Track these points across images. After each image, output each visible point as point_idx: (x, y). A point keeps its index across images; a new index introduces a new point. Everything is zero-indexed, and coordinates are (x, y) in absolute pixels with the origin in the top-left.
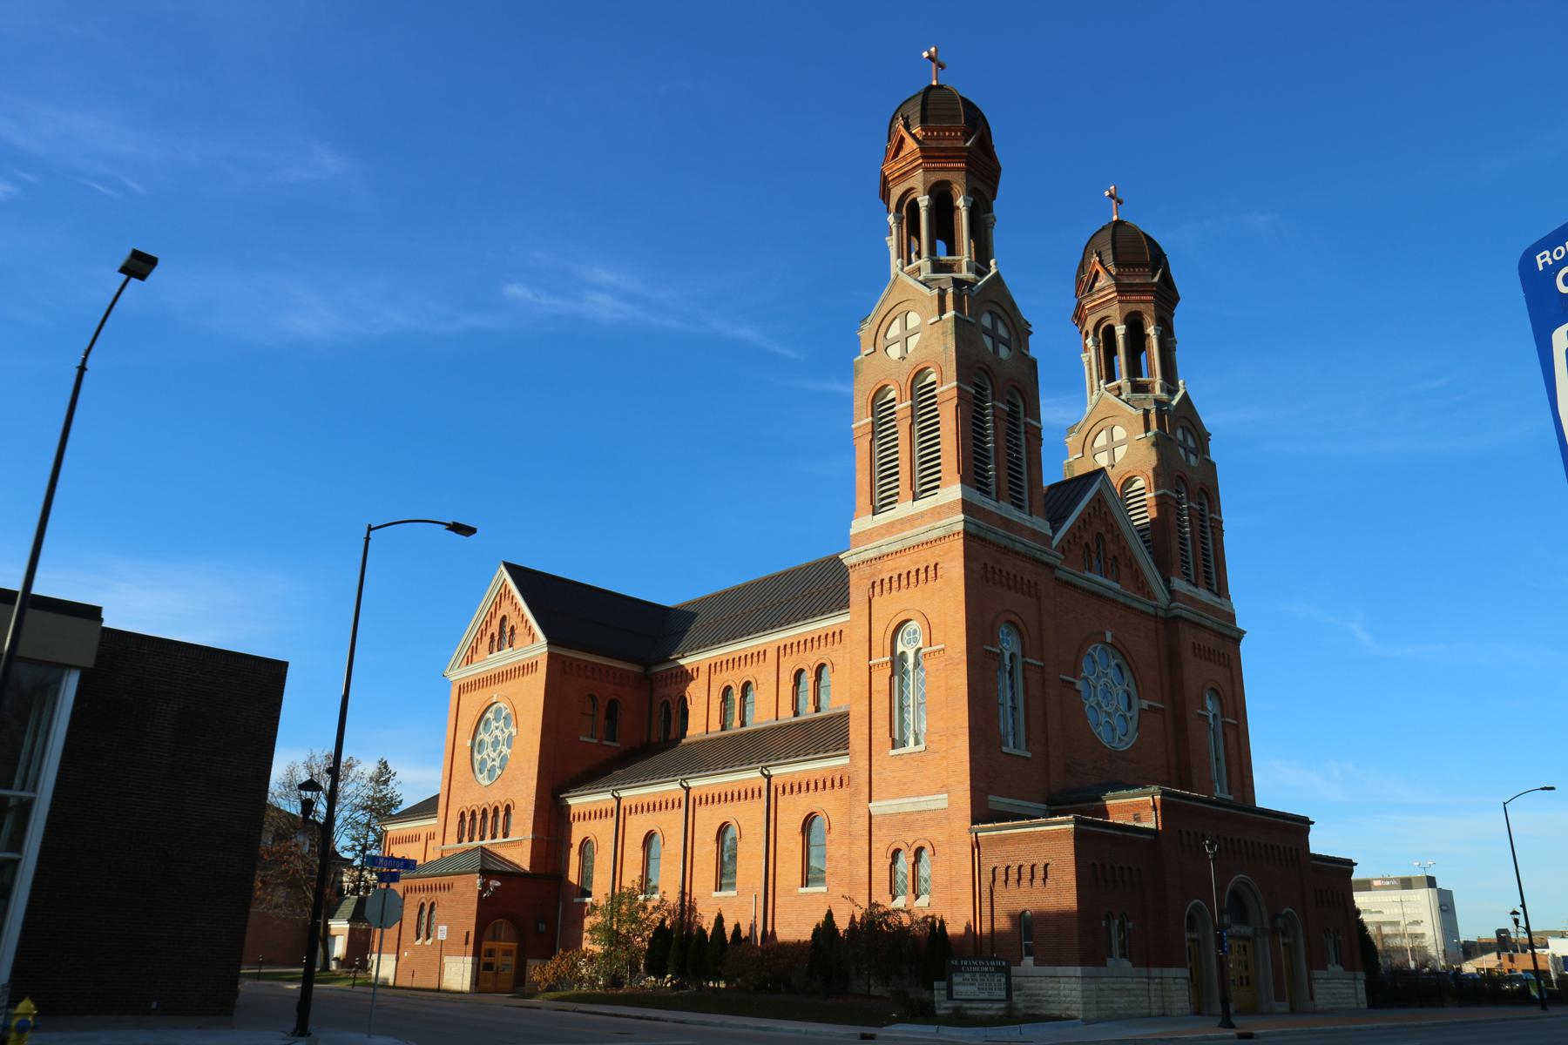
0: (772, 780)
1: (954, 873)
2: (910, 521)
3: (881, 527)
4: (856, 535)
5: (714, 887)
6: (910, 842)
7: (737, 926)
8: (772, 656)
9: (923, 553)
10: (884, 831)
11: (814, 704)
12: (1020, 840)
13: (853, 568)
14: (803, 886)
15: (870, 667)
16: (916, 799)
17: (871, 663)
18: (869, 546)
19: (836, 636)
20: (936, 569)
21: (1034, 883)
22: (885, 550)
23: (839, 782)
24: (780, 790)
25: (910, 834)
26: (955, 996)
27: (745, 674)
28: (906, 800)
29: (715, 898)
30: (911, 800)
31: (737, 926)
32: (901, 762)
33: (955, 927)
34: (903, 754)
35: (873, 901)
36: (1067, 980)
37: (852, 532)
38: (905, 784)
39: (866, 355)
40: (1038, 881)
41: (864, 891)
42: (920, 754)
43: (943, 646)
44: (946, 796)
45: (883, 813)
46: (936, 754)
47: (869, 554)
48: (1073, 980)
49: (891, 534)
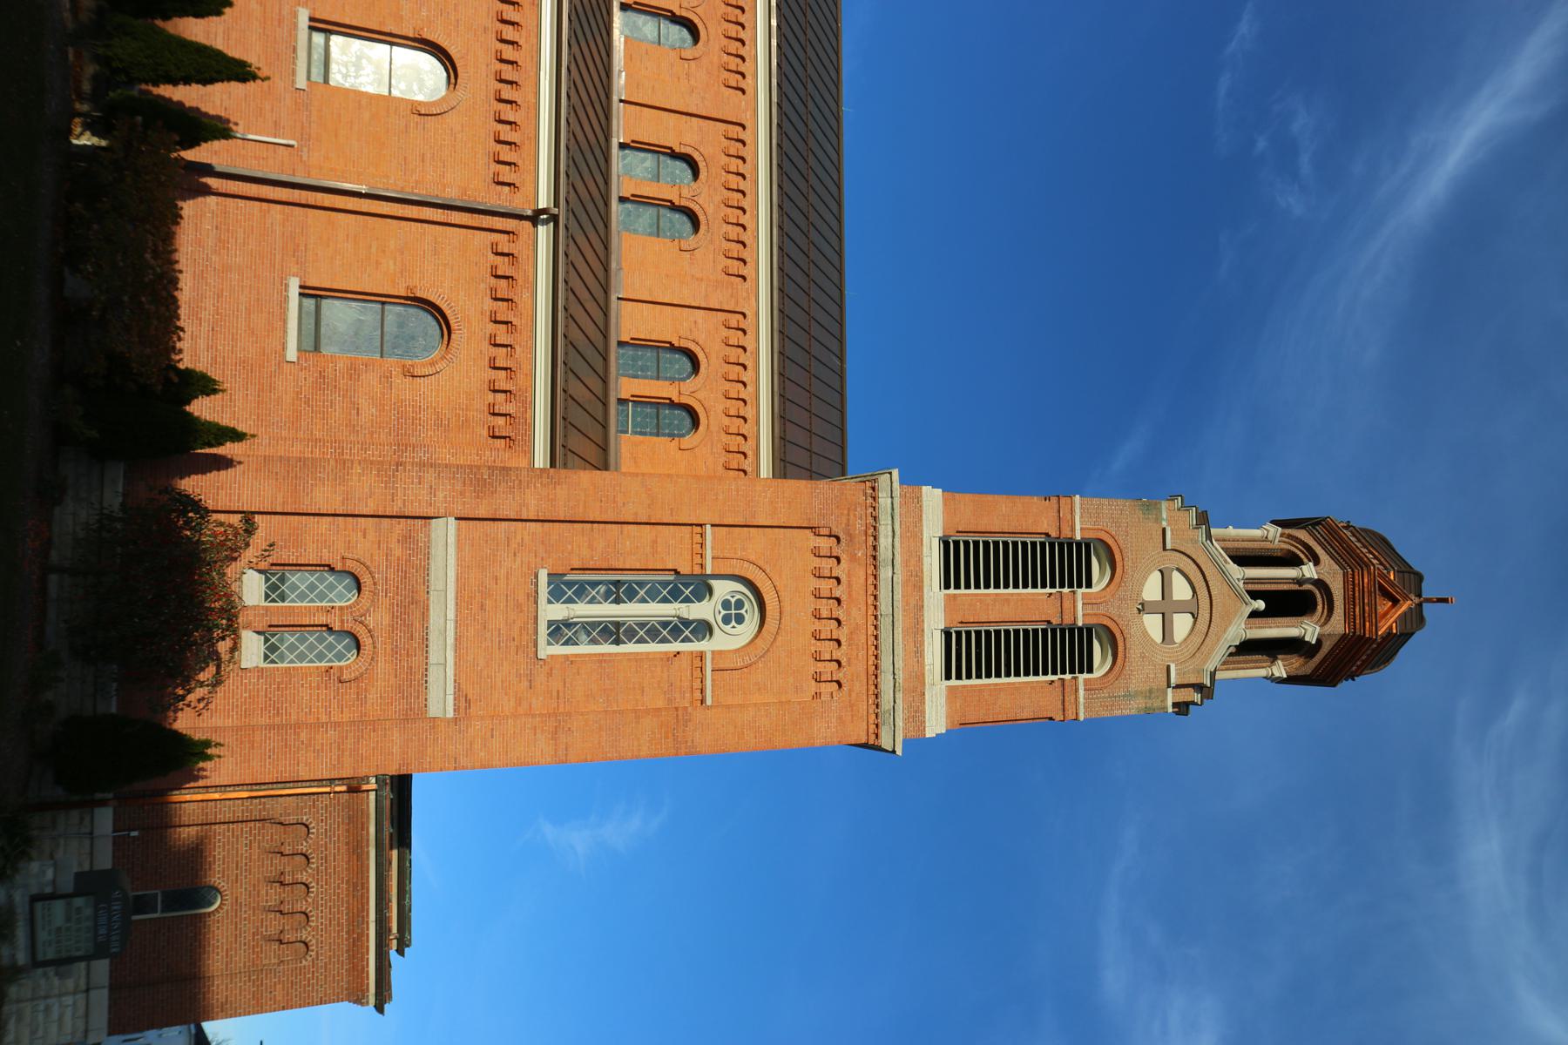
0: (527, 224)
1: (303, 736)
2: (917, 611)
3: (920, 560)
4: (919, 499)
5: (309, 284)
6: (370, 620)
7: (219, 129)
8: (731, 106)
9: (862, 653)
10: (398, 552)
11: (633, 195)
12: (355, 886)
13: (869, 491)
14: (312, 19)
15: (701, 525)
16: (450, 640)
17: (708, 527)
18: (897, 501)
19: (738, 268)
20: (737, 89)
21: (272, 915)
22: (885, 573)
23: (507, 431)
24: (504, 243)
25: (386, 620)
26: (39, 906)
27: (712, 31)
28: (451, 615)
29: (295, 15)
30: (451, 626)
31: (219, 129)
32: (522, 598)
33: (189, 801)
34: (536, 603)
35: (257, 518)
36: (81, 1011)
37: (926, 489)
38: (482, 607)
39: (1164, 530)
40: (273, 924)
41: (280, 500)
42: (531, 645)
43: (709, 702)
44: (450, 714)
45: (433, 551)
46: (526, 684)
47: (887, 537)
48: (81, 1025)
49: (905, 583)
